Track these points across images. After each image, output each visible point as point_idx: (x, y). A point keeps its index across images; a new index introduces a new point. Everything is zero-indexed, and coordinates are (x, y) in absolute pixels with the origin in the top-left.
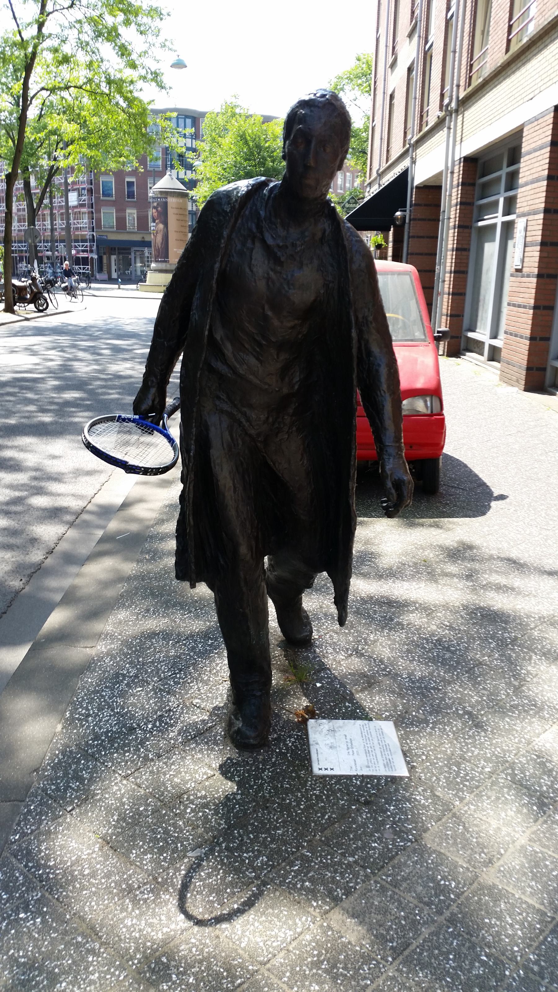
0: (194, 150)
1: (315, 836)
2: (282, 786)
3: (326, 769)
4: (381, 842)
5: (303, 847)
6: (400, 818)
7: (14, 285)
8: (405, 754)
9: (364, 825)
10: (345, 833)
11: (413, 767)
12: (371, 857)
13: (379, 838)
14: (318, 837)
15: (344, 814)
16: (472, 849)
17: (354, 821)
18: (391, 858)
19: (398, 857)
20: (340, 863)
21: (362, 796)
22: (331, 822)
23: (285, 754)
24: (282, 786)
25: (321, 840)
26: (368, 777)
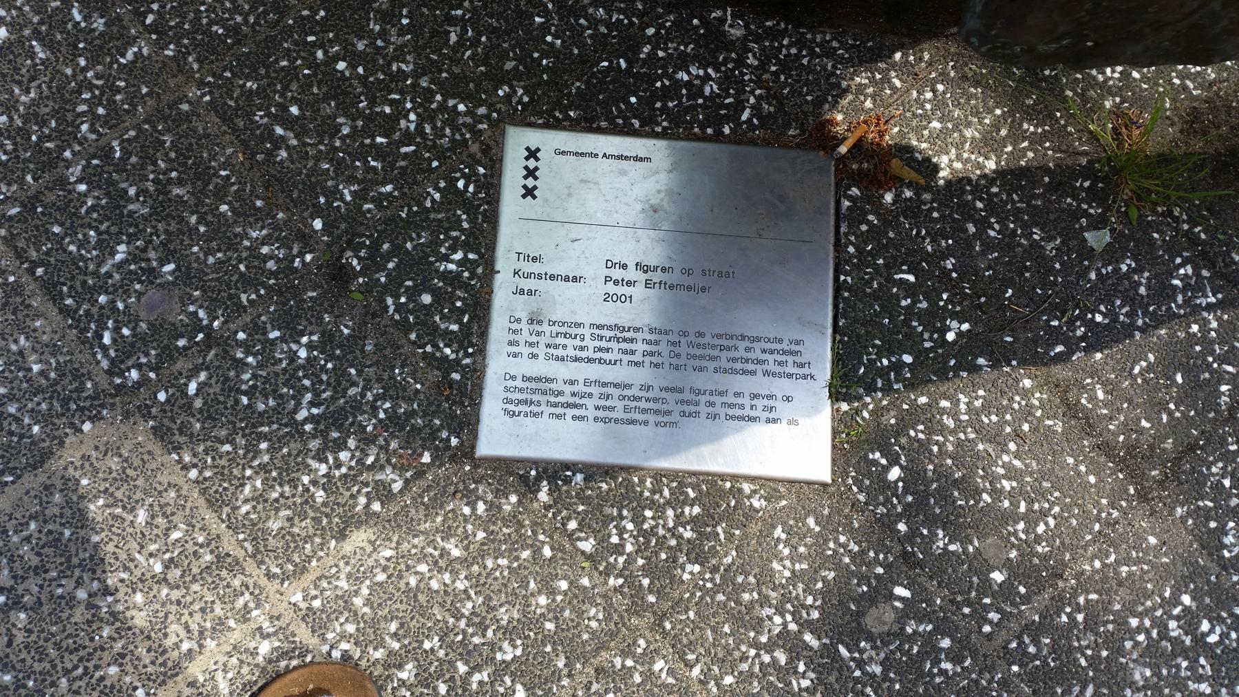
0: (530, 345)
1: (201, 84)
2: (453, 21)
3: (531, 173)
4: (131, 277)
5: (160, 45)
6: (240, 365)
7: (1233, 366)
8: (594, 472)
9: (222, 236)
10: (200, 176)
11: (528, 487)
12: (71, 231)
13: (152, 273)
14: (193, 92)
15: (290, 190)
16: (40, 570)
17: (245, 213)
18: (50, 289)
19: (53, 312)
20: (67, 135)
21: (374, 262)
22: (255, 143)
23: (631, 53)
24: (453, 21)
25: (183, 98)
26: (480, 308)
